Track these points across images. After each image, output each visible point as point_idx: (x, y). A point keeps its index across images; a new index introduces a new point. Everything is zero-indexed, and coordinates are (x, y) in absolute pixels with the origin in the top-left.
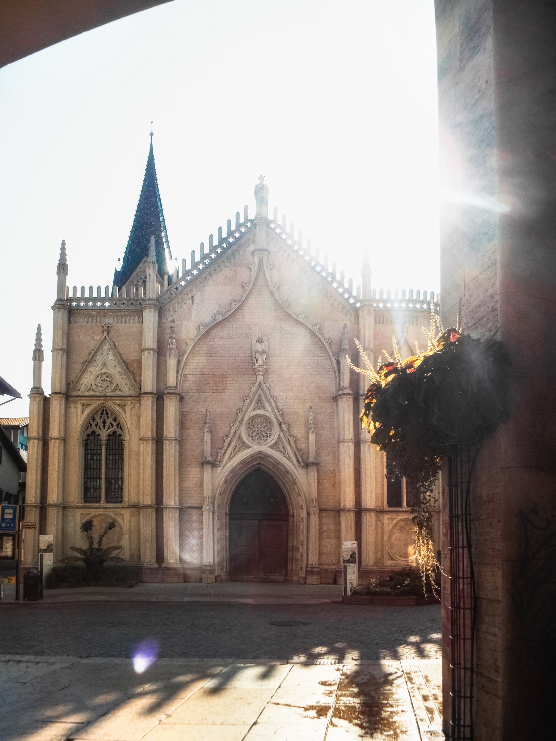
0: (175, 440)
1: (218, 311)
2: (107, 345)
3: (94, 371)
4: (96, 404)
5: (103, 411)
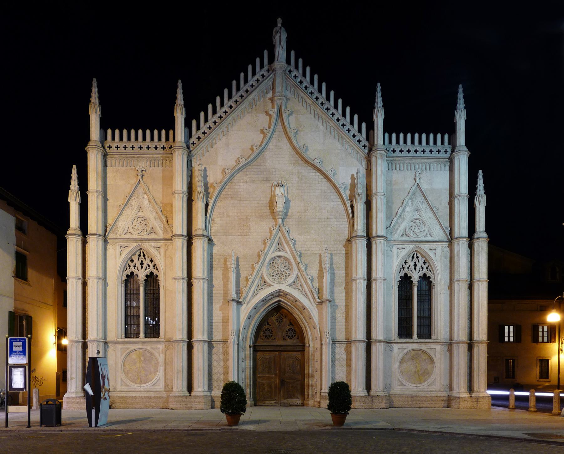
0: (203, 279)
4: (133, 245)
5: (140, 253)
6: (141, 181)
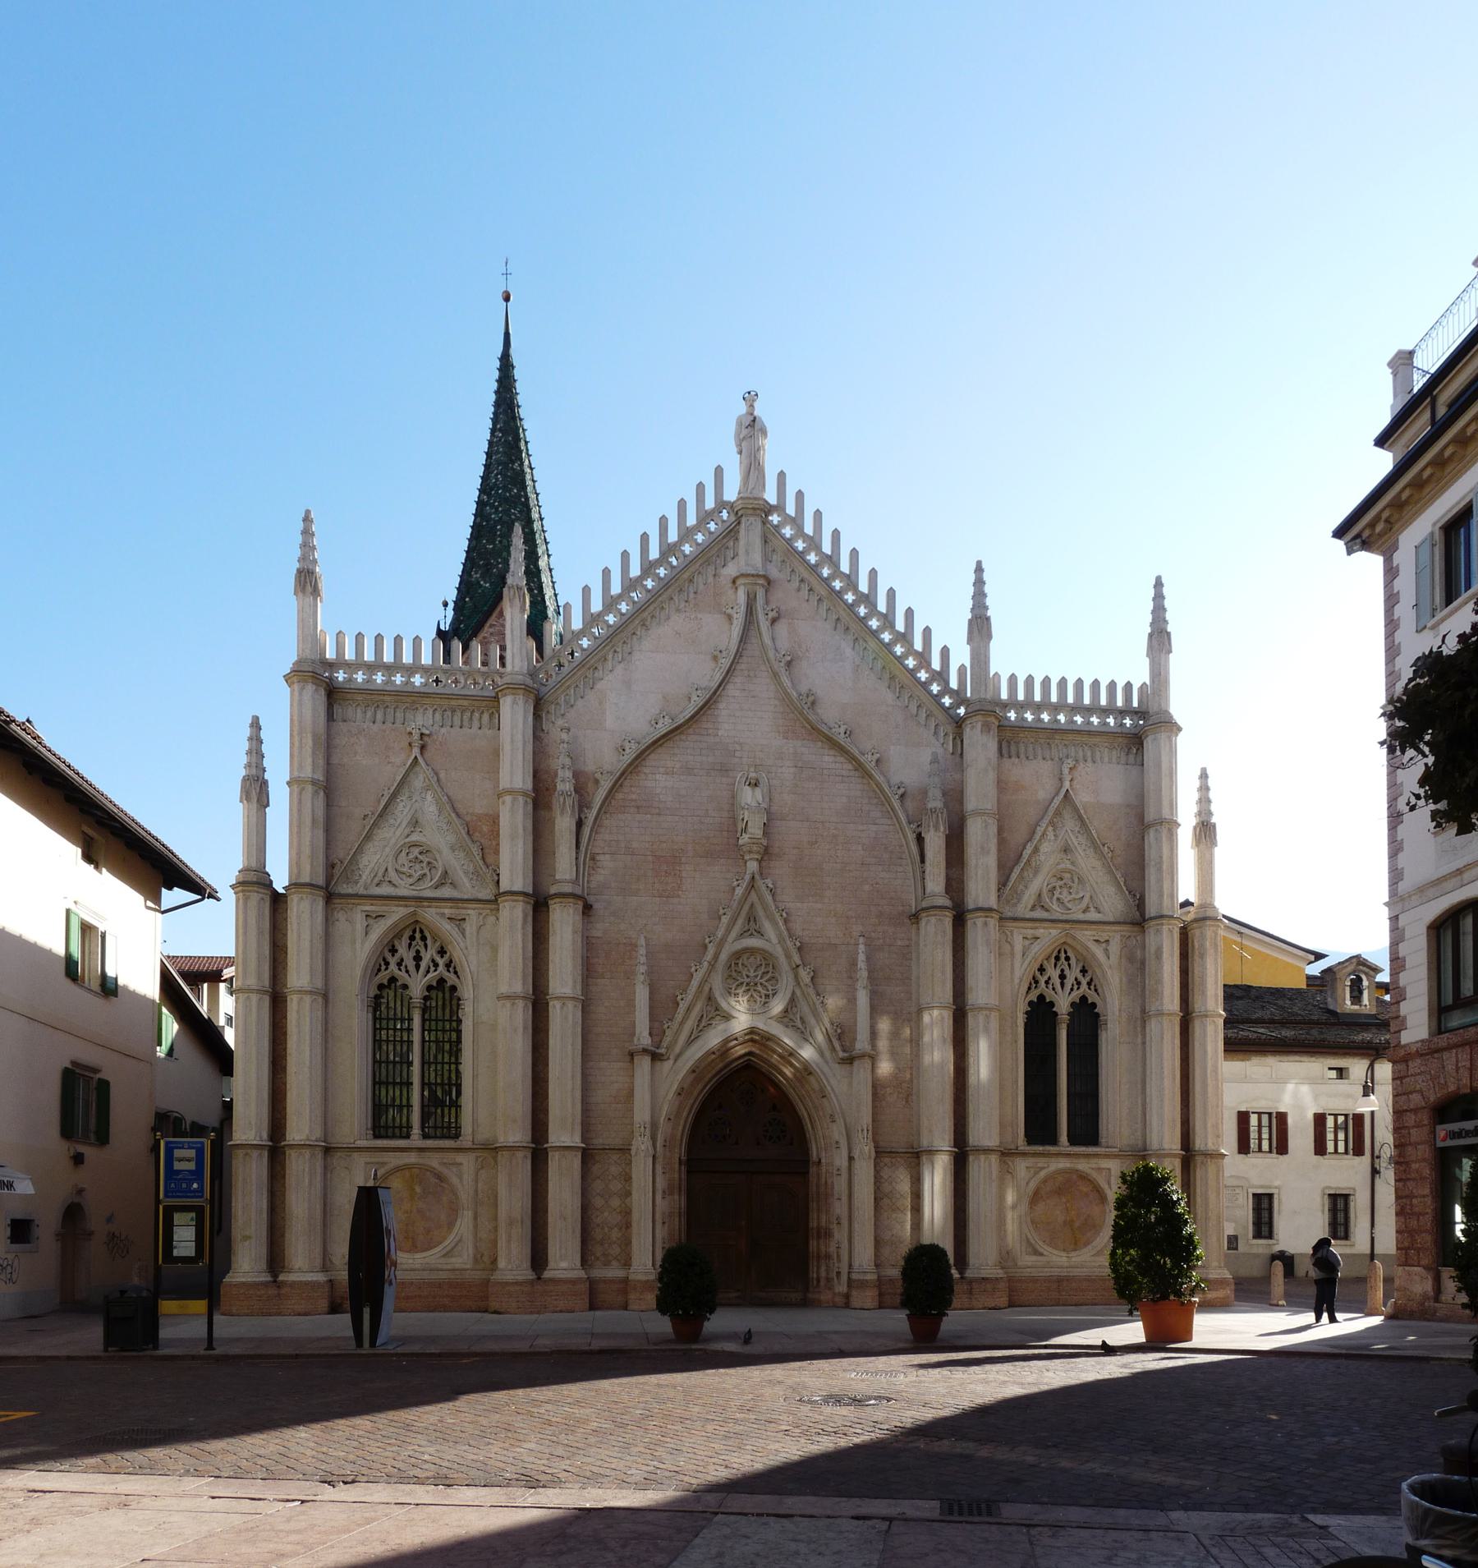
1: (661, 711)
2: (421, 777)
3: (392, 834)
4: (397, 913)
5: (414, 931)
6: (420, 759)
